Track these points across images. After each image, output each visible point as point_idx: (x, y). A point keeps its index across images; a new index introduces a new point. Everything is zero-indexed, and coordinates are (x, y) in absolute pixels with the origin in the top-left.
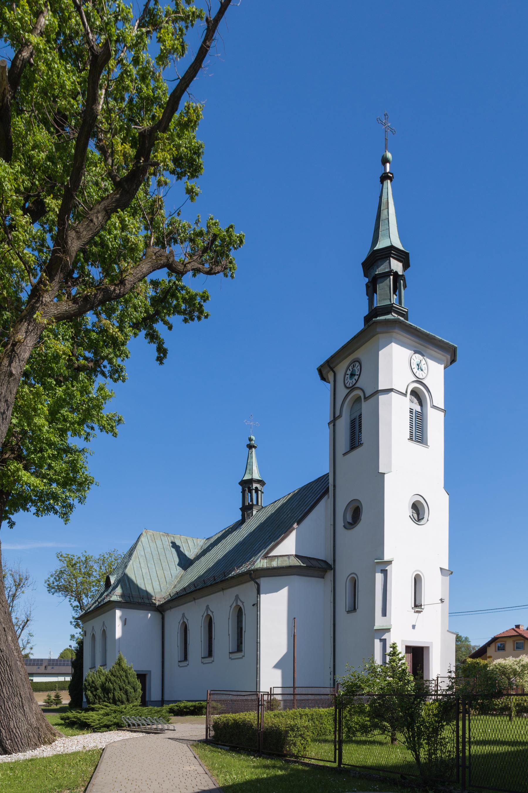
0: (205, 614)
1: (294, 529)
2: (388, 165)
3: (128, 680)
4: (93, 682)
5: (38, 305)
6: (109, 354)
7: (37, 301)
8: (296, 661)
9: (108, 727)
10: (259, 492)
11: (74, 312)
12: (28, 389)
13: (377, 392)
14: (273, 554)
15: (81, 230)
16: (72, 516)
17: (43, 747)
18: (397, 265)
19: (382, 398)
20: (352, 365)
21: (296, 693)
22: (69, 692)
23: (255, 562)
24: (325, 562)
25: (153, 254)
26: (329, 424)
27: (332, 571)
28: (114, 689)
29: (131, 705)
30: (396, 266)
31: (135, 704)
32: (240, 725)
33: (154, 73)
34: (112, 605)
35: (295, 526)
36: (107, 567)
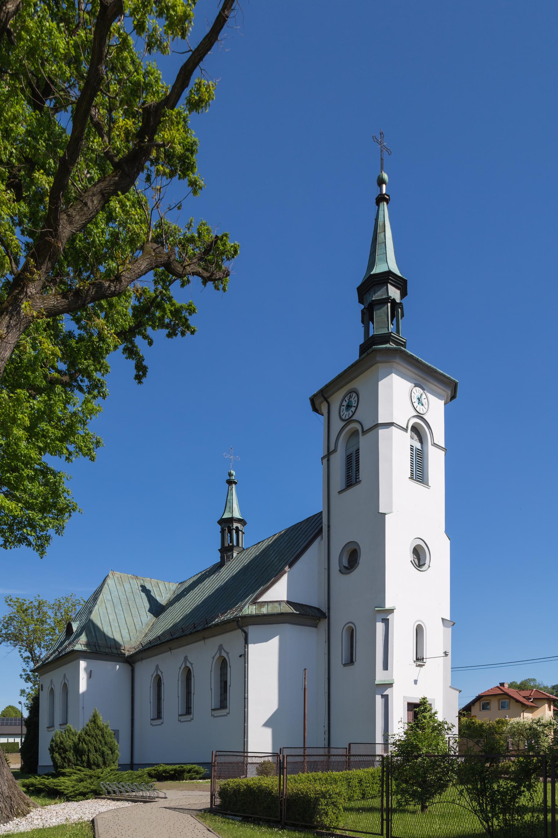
0: (183, 666)
1: (285, 572)
2: (384, 186)
3: (104, 740)
4: (61, 743)
5: (22, 297)
6: (89, 366)
7: (21, 292)
8: (306, 718)
9: (84, 795)
10: (240, 532)
11: (63, 309)
12: (8, 395)
13: (377, 426)
14: (263, 599)
15: (74, 214)
16: (48, 549)
17: (16, 820)
18: (395, 292)
19: (382, 432)
20: (348, 396)
21: (306, 754)
22: (21, 755)
23: (243, 608)
24: (318, 609)
25: (152, 250)
26: (322, 459)
27: (327, 619)
28: (89, 750)
29: (108, 769)
30: (394, 293)
31: (113, 767)
32: (254, 792)
33: (161, 43)
34: (76, 655)
35: (287, 568)
36: (63, 614)
